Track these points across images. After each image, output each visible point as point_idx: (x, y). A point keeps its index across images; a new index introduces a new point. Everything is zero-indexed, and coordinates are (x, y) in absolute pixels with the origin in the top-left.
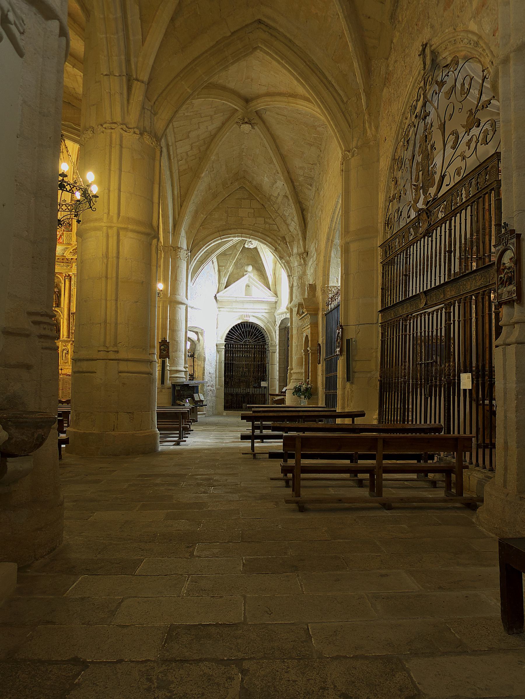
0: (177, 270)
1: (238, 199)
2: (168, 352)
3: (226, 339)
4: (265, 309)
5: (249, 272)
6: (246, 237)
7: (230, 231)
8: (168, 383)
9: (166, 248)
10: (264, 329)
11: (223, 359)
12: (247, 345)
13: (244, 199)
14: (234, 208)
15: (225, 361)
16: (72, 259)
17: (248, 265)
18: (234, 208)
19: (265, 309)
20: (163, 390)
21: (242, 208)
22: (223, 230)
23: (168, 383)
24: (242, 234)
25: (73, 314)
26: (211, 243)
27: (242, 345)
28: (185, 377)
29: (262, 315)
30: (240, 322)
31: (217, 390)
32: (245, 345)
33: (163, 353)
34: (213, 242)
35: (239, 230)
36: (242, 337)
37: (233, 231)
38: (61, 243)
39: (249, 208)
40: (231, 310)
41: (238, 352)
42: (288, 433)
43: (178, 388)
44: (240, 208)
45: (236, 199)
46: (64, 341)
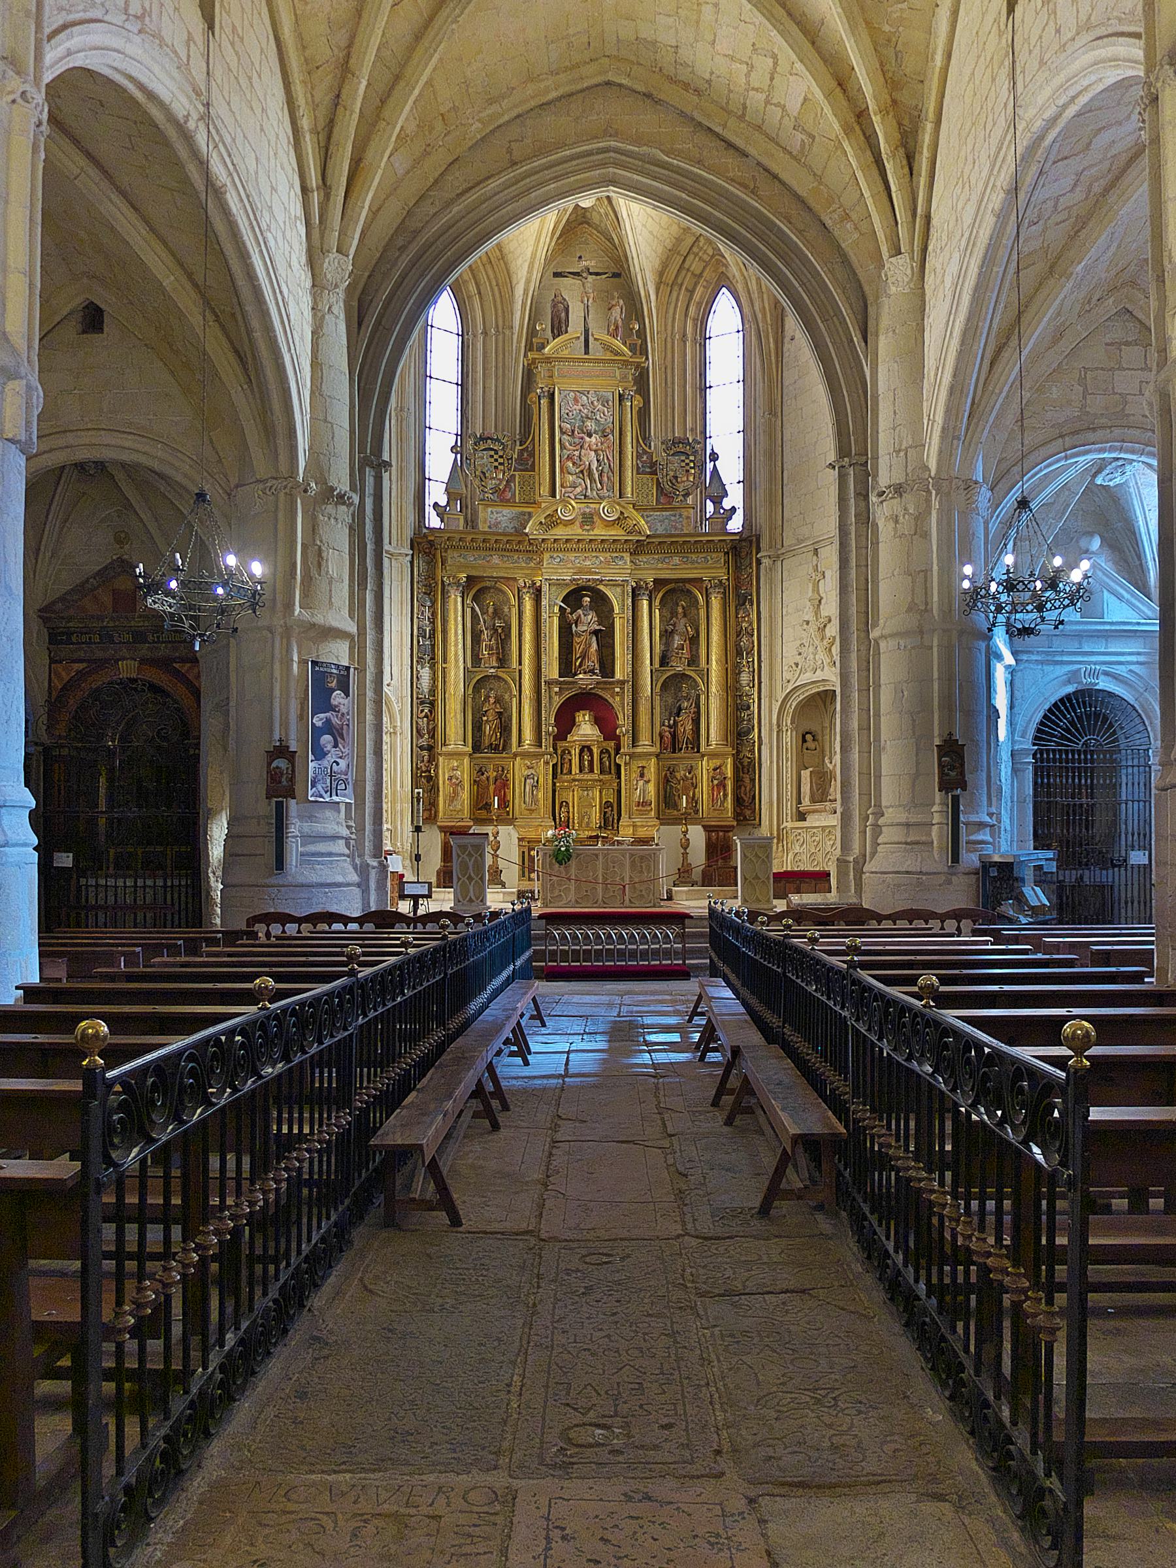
0: (970, 543)
1: (1112, 344)
2: (962, 773)
3: (1036, 738)
4: (1139, 654)
5: (1093, 553)
6: (1133, 452)
7: (1091, 436)
8: (970, 859)
9: (945, 484)
10: (1134, 709)
11: (1030, 791)
12: (1092, 753)
13: (1127, 344)
14: (1102, 369)
15: (1035, 795)
16: (543, 540)
17: (1091, 534)
18: (1102, 369)
19: (1139, 654)
20: (954, 878)
21: (1125, 369)
22: (1073, 433)
23: (970, 859)
24: (1123, 441)
25: (549, 683)
26: (1041, 470)
27: (1079, 751)
28: (991, 840)
29: (1130, 671)
30: (1070, 689)
31: (231, 855)
32: (1085, 753)
33: (948, 775)
34: (1046, 467)
35: (1117, 432)
36: (1077, 730)
37: (1100, 434)
38: (508, 501)
39: (1142, 369)
40: (1049, 658)
41: (1067, 772)
42: (1144, 983)
43: (994, 873)
44: (1118, 369)
45: (1107, 344)
46: (525, 755)
